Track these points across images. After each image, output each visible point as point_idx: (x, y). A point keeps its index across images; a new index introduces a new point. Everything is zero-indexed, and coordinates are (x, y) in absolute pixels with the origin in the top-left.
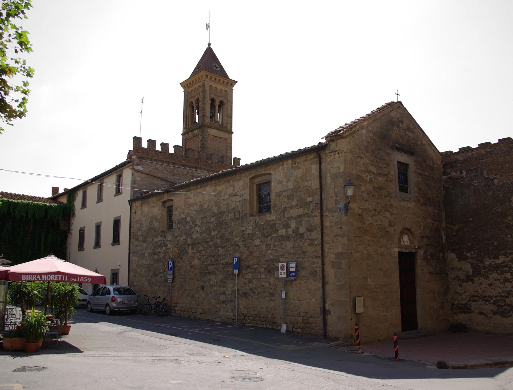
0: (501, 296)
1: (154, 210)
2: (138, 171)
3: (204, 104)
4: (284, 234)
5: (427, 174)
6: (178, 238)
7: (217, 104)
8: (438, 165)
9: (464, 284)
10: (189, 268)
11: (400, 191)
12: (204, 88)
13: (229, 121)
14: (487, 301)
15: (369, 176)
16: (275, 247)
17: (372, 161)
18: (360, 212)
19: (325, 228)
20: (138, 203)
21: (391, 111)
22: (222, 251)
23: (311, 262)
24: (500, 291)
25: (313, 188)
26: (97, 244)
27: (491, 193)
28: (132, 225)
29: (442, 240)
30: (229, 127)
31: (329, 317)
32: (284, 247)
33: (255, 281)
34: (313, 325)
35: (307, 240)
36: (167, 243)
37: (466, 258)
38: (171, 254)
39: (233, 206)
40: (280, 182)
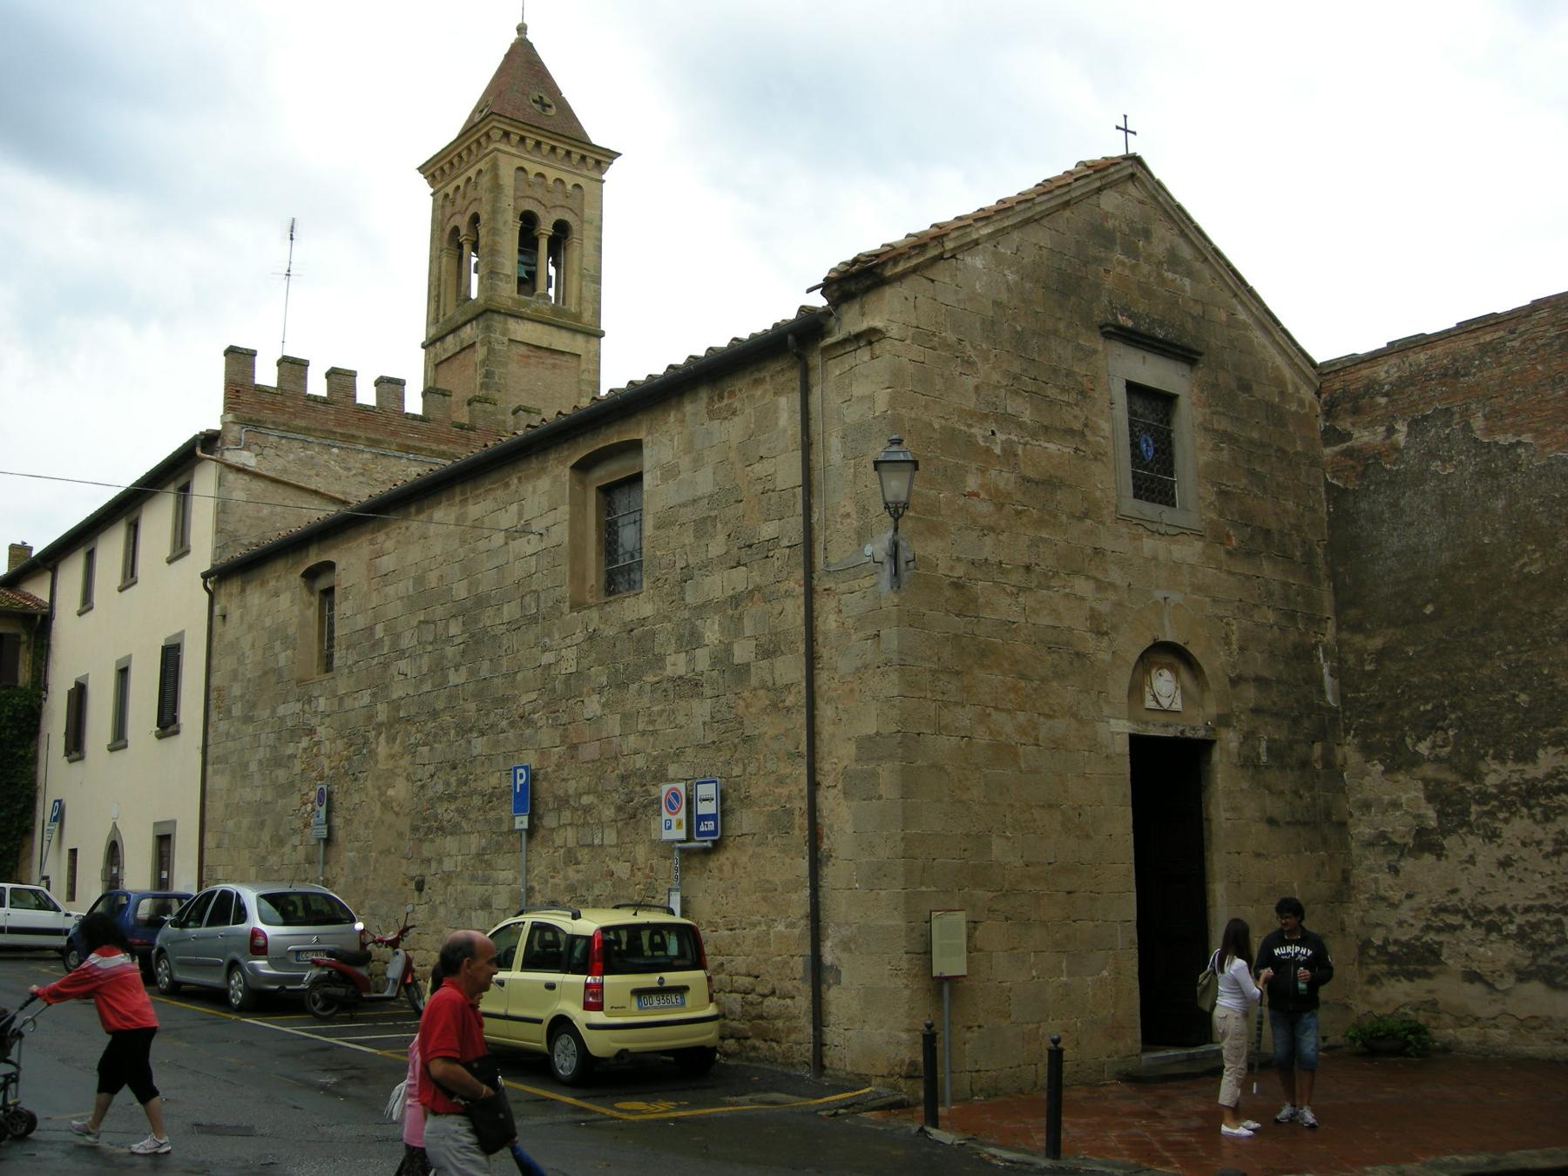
0: (1547, 909)
1: (280, 600)
2: (241, 470)
3: (494, 232)
4: (681, 671)
5: (1255, 435)
6: (348, 703)
7: (546, 228)
8: (1301, 402)
9: (1407, 864)
10: (377, 813)
11: (1136, 496)
12: (496, 177)
13: (587, 294)
14: (1492, 927)
15: (1000, 437)
16: (652, 722)
17: (1016, 378)
18: (960, 571)
19: (820, 639)
20: (234, 586)
21: (1099, 190)
22: (479, 745)
23: (772, 778)
24: (1543, 888)
25: (780, 485)
26: (119, 740)
27: (1500, 504)
28: (214, 662)
29: (1322, 692)
31: (832, 995)
32: (681, 720)
33: (583, 855)
34: (780, 1024)
35: (761, 692)
36: (314, 721)
37: (1416, 760)
38: (326, 763)
39: (517, 571)
40: (670, 472)
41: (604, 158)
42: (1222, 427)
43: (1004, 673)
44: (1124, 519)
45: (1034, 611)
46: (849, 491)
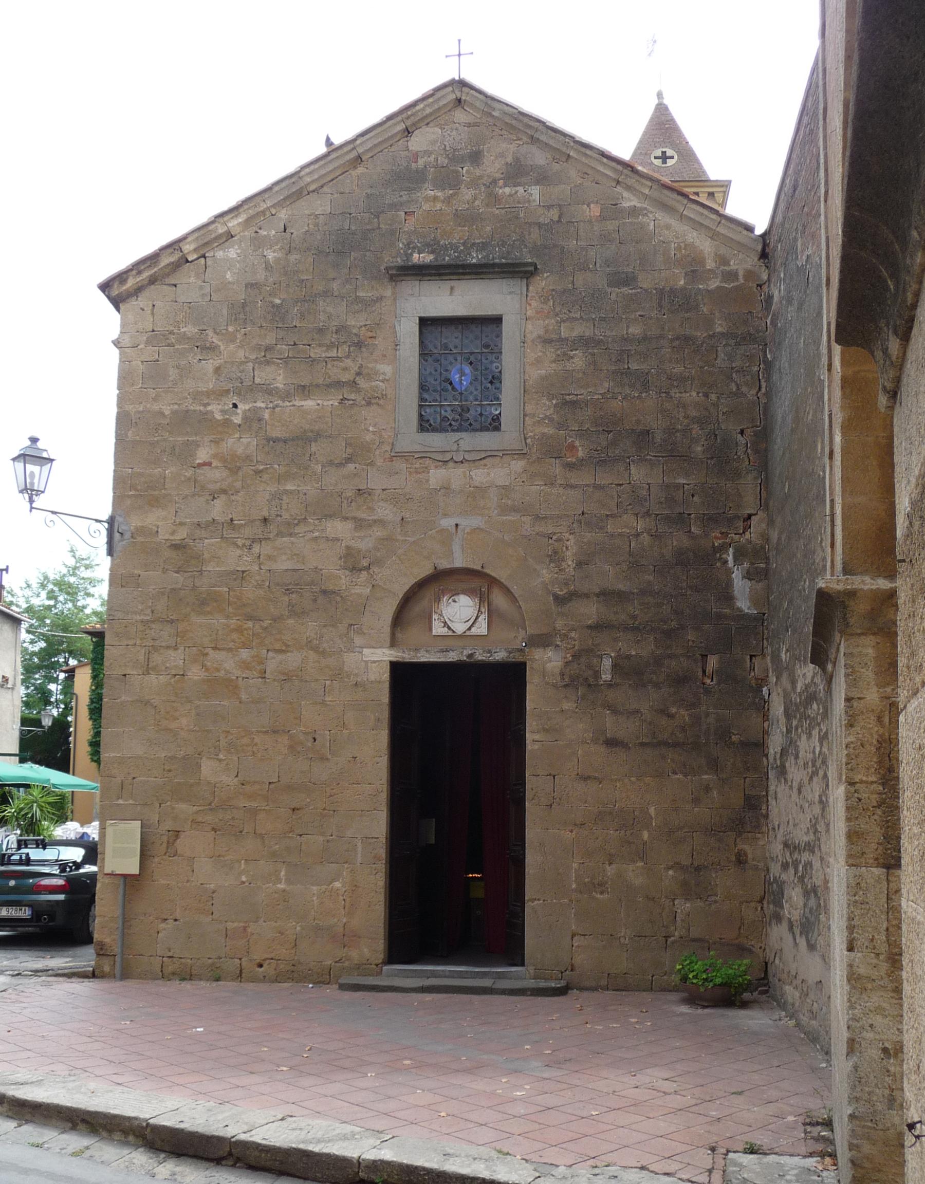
42: (575, 333)
43: (228, 617)
44: (404, 456)
45: (270, 558)
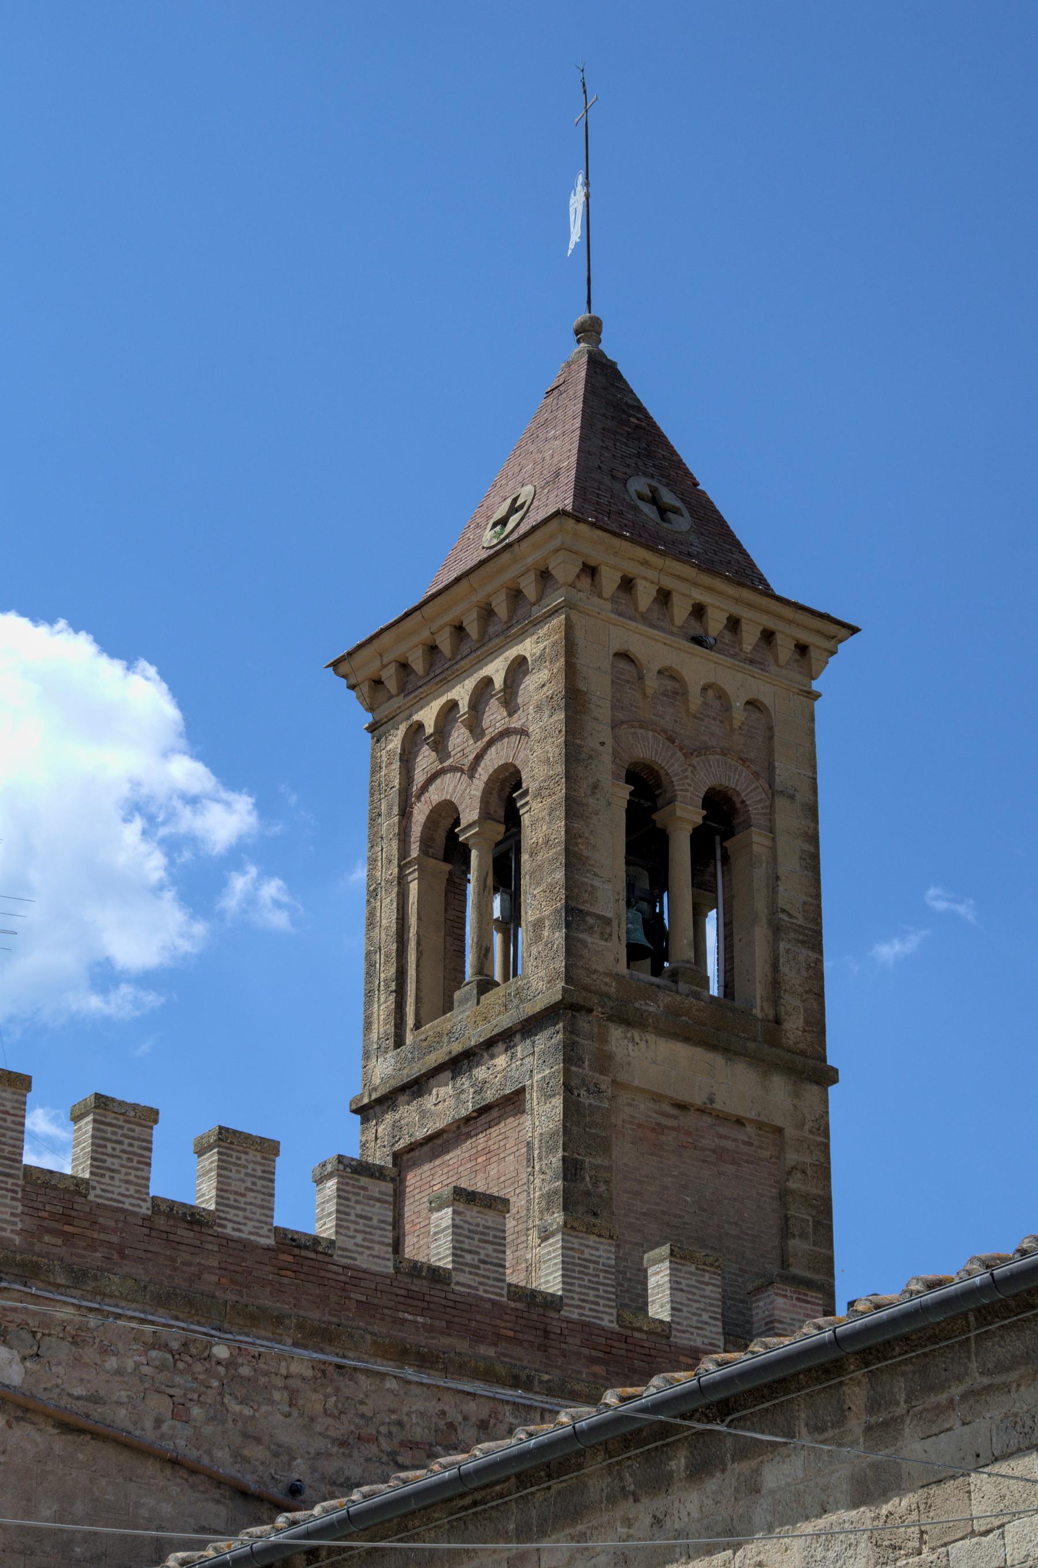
7: (685, 816)
13: (792, 975)
30: (794, 1026)
41: (813, 637)
46: (535, 1084)
